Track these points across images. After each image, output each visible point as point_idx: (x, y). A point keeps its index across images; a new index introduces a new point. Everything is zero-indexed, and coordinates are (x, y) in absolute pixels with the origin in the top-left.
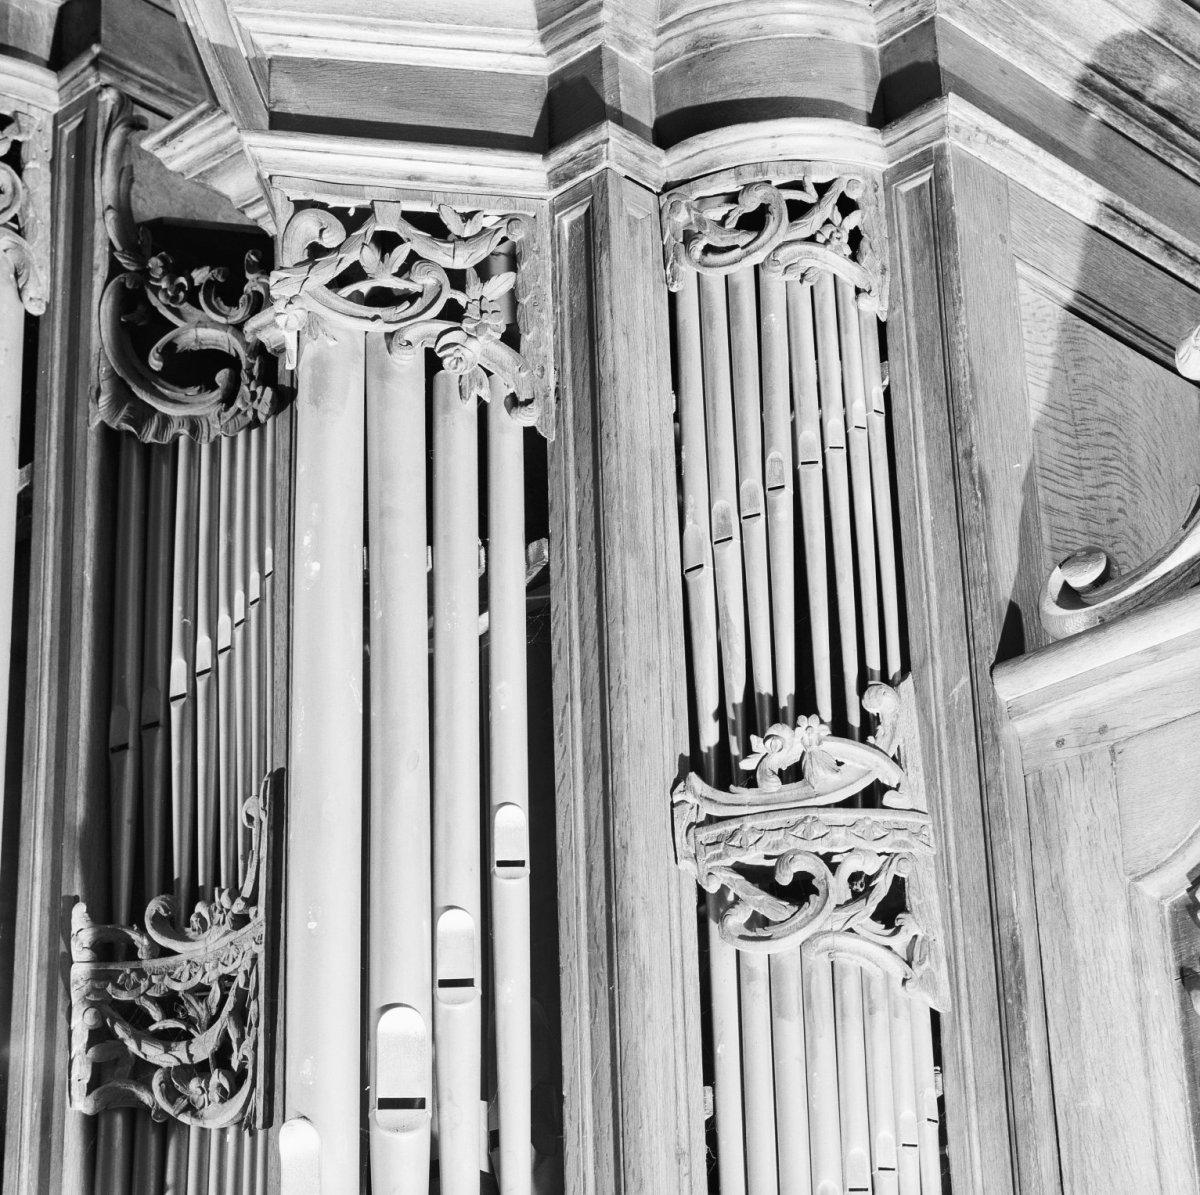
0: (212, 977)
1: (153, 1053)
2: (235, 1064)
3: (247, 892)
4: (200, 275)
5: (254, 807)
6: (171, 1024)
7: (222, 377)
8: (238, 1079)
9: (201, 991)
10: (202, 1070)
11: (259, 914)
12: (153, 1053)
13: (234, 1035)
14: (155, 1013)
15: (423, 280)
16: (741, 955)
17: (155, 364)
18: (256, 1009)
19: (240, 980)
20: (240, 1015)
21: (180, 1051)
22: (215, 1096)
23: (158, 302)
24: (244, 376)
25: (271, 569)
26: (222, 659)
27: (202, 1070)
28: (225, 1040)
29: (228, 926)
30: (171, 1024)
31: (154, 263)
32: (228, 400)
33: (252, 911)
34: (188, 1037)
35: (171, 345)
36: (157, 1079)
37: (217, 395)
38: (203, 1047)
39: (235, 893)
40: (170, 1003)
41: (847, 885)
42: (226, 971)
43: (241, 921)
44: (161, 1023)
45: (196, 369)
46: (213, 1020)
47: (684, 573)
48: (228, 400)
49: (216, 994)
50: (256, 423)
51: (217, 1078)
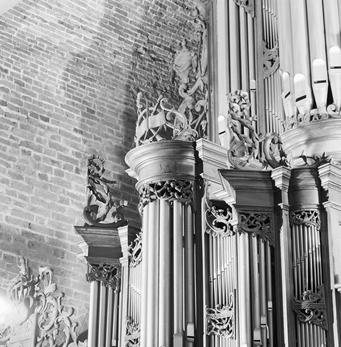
0: (226, 317)
1: (218, 327)
2: (230, 330)
3: (231, 305)
4: (220, 211)
5: (232, 294)
6: (220, 323)
7: (224, 227)
8: (231, 332)
9: (224, 319)
10: (224, 330)
11: (233, 309)
12: (218, 327)
13: (230, 326)
14: (218, 321)
15: (257, 223)
16: (240, 88)
17: (214, 224)
18: (233, 323)
19: (230, 318)
20: (231, 323)
21: (221, 327)
22: (227, 334)
23: (214, 214)
24: (228, 229)
25: (24, 290)
26: (225, 270)
27: (224, 330)
28: (228, 326)
29: (228, 310)
30: (220, 323)
31: (213, 208)
32: (225, 231)
33: (232, 309)
34: (222, 325)
35: (216, 221)
36: (219, 331)
37: (224, 230)
38: (225, 326)
39: (229, 306)
40: (220, 320)
41: (196, 83)
42: (229, 316)
43: (230, 310)
44: (218, 323)
45: (220, 225)
46: (226, 323)
47: (293, 267)
48: (225, 231)
49: (226, 319)
50: (230, 236)
51: (227, 332)
